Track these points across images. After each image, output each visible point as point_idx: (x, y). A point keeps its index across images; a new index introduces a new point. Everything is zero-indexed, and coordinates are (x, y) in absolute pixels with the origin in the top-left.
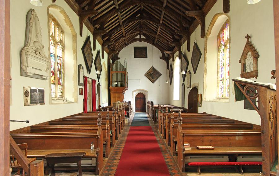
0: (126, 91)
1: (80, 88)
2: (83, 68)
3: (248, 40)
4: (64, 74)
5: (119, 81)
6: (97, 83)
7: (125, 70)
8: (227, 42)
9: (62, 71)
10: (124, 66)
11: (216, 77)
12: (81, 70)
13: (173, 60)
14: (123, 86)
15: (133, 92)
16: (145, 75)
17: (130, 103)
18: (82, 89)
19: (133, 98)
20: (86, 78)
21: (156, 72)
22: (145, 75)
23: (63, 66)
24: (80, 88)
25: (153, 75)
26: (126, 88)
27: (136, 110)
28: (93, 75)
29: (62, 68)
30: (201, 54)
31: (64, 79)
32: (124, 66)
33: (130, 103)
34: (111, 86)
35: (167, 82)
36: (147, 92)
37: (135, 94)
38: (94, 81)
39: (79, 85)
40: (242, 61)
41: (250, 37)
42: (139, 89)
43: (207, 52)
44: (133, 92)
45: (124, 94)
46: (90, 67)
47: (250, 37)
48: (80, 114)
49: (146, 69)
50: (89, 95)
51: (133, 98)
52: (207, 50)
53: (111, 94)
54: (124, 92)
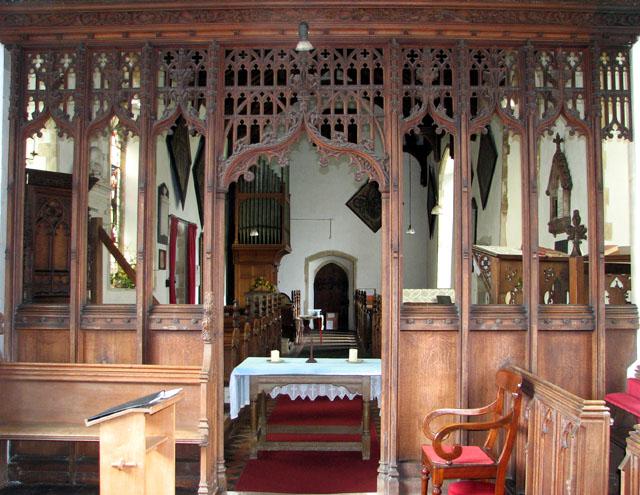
0: (284, 257)
1: (160, 251)
2: (167, 194)
3: (558, 147)
4: (122, 212)
5: (274, 227)
6: (199, 231)
7: (282, 188)
8: (623, 65)
9: (118, 203)
10: (280, 176)
11: (174, 334)
12: (164, 198)
13: (439, 158)
14: (276, 244)
15: (309, 260)
16: (347, 204)
17: (296, 295)
18: (165, 252)
19: (307, 281)
20: (174, 220)
21: (253, 383)
22: (347, 204)
23: (122, 189)
24: (160, 251)
25: (367, 205)
26: (284, 246)
27: (375, 358)
28: (189, 213)
29: (118, 195)
30: (496, 157)
31: (121, 226)
32: (280, 176)
33: (296, 295)
34: (236, 242)
35: (412, 232)
36: (353, 261)
37: (314, 266)
38: (191, 228)
39: (159, 242)
40: (551, 192)
41: (562, 140)
42: (328, 252)
43: (508, 153)
44: (309, 260)
45: (276, 266)
46: (183, 188)
47: (562, 140)
48: (538, 243)
49: (351, 190)
50: (179, 270)
51: (307, 281)
52: (508, 147)
53: (236, 266)
54: (279, 262)
